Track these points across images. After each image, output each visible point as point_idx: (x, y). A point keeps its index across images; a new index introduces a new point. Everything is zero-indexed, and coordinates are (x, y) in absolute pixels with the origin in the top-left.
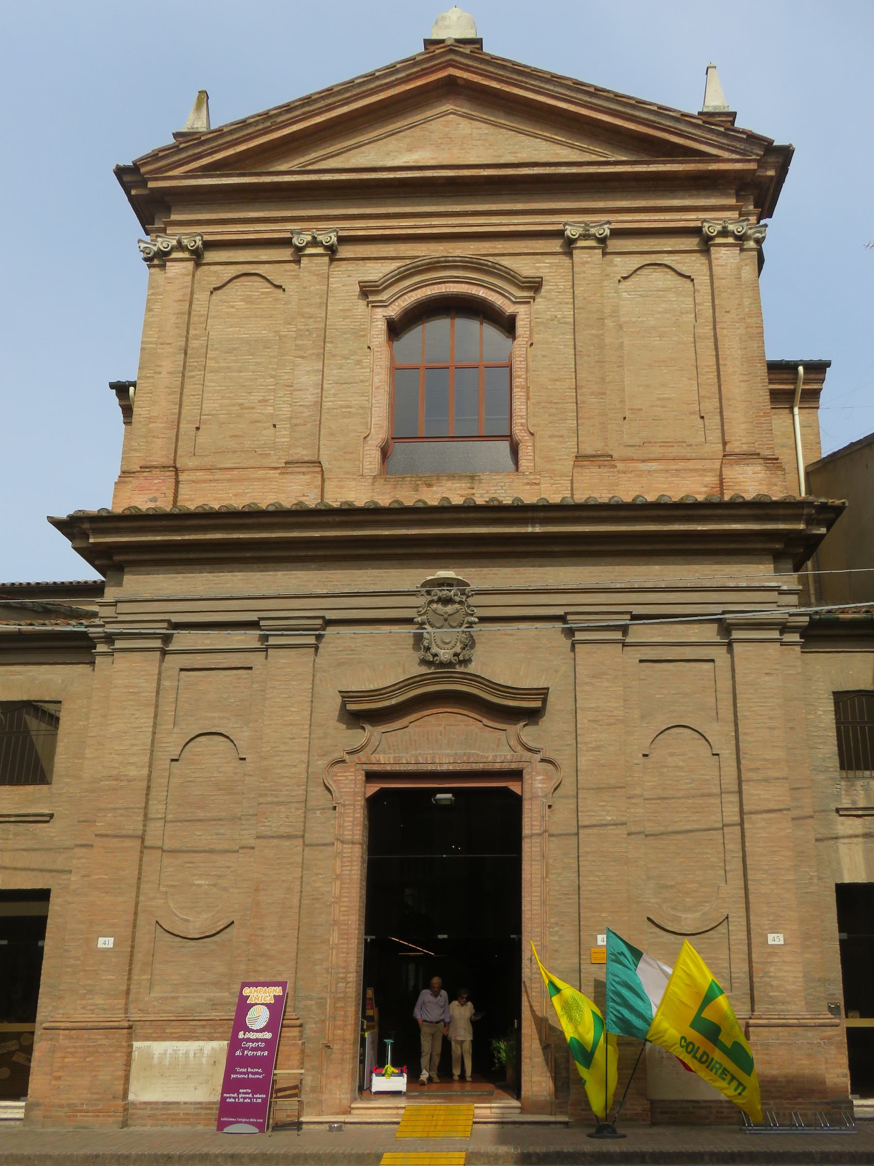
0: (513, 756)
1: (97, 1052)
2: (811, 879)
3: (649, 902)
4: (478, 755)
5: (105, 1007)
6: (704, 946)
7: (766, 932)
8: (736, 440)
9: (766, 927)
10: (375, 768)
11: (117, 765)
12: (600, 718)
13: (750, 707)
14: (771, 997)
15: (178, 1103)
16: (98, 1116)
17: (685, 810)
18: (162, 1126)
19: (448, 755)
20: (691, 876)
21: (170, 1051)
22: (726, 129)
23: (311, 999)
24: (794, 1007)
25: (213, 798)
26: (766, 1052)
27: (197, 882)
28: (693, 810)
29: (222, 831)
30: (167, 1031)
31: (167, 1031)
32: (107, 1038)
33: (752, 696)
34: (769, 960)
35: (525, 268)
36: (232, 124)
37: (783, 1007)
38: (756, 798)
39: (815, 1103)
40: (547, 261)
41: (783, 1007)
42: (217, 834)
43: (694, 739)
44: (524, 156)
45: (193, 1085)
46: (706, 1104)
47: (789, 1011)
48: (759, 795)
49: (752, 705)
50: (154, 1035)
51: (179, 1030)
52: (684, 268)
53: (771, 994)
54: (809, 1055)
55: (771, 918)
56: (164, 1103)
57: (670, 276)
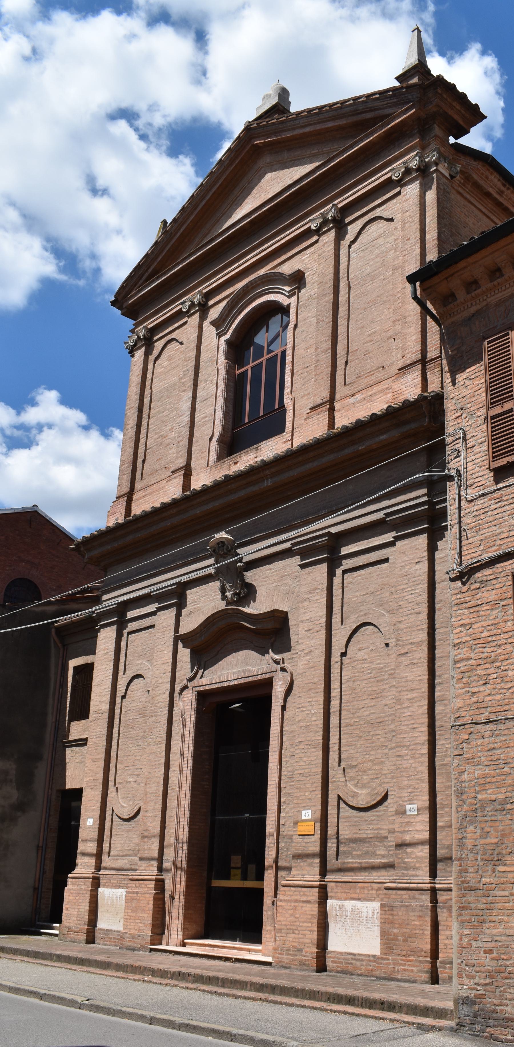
0: (267, 667)
1: (80, 893)
2: (446, 751)
3: (339, 781)
4: (249, 670)
5: (89, 864)
6: (373, 818)
7: (405, 803)
8: (408, 353)
9: (406, 799)
10: (202, 689)
11: (98, 703)
12: (311, 627)
13: (404, 597)
14: (405, 863)
15: (111, 930)
16: (78, 935)
17: (366, 697)
18: (105, 945)
19: (234, 673)
20: (367, 756)
21: (111, 896)
22: (277, 119)
23: (168, 862)
24: (421, 872)
25: (137, 720)
26: (391, 912)
27: (129, 780)
28: (371, 697)
29: (140, 744)
30: (112, 881)
31: (112, 881)
32: (84, 885)
33: (406, 586)
34: (406, 830)
35: (287, 269)
36: (152, 247)
37: (414, 873)
38: (404, 680)
39: (420, 961)
40: (308, 253)
41: (414, 873)
42: (138, 746)
43: (374, 632)
44: (297, 177)
45: (118, 919)
46: (361, 957)
47: (417, 876)
48: (406, 677)
49: (405, 594)
50: (107, 884)
51: (115, 882)
52: (389, 213)
53: (406, 860)
54: (420, 916)
55: (409, 790)
56: (107, 930)
57: (382, 223)
